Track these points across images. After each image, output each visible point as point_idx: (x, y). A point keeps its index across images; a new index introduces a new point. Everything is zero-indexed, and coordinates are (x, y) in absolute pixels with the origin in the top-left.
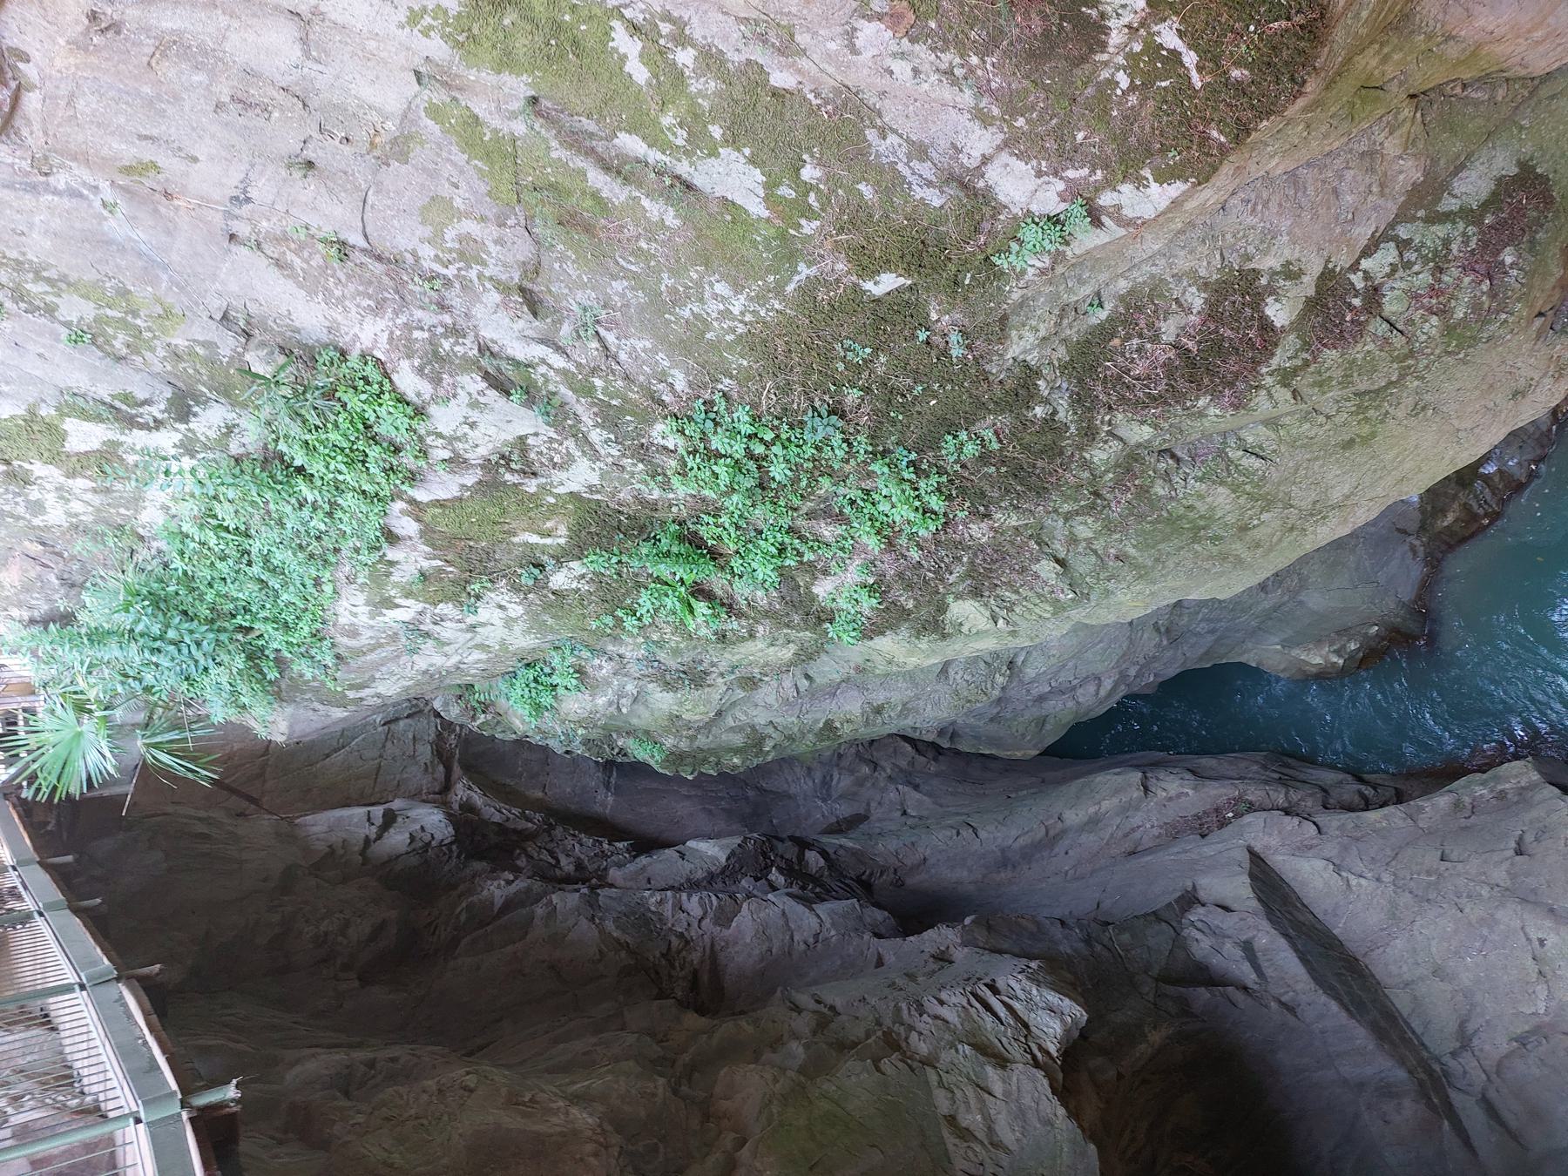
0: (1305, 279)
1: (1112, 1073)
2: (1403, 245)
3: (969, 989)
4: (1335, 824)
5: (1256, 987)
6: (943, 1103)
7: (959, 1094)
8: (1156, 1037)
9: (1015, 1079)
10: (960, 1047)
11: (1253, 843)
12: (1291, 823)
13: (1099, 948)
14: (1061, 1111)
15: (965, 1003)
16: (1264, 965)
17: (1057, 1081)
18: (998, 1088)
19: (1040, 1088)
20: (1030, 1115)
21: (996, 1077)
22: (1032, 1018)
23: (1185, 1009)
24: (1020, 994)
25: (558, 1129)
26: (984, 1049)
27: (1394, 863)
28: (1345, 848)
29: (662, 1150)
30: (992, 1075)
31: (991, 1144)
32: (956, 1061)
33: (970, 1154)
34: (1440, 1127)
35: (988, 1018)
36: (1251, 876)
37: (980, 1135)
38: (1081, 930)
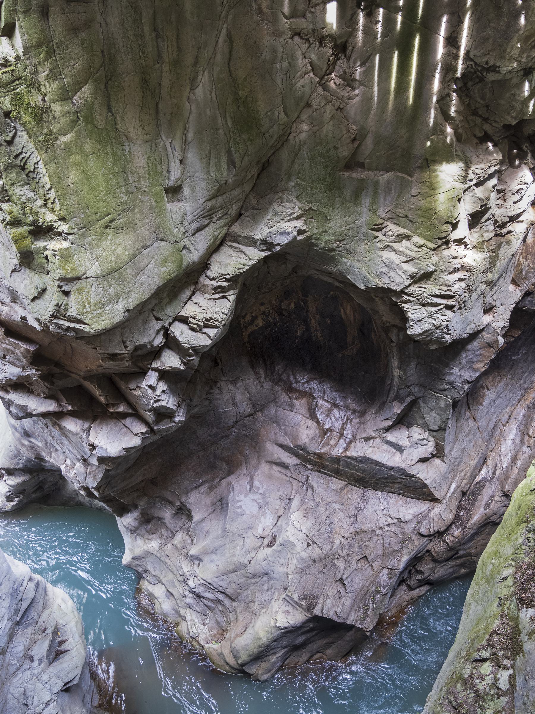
0: (527, 638)
1: (394, 338)
2: (500, 693)
3: (457, 297)
4: (417, 543)
5: (384, 435)
6: (417, 239)
7: (415, 249)
8: (396, 373)
9: (403, 276)
10: (433, 267)
11: (440, 505)
12: (434, 527)
13: (446, 386)
14: (380, 284)
15: (452, 289)
16: (390, 448)
17: (394, 296)
18: (406, 266)
19: (394, 284)
20: (387, 270)
21: (409, 269)
22: (424, 310)
23: (399, 398)
24: (438, 315)
25: (508, 50)
26: (427, 276)
27: (382, 542)
28: (403, 533)
29: (481, 102)
30: (411, 269)
31: (388, 246)
32: (429, 260)
33: (391, 234)
34: (292, 442)
35: (438, 292)
36: (425, 486)
37: (394, 245)
38: (458, 387)
